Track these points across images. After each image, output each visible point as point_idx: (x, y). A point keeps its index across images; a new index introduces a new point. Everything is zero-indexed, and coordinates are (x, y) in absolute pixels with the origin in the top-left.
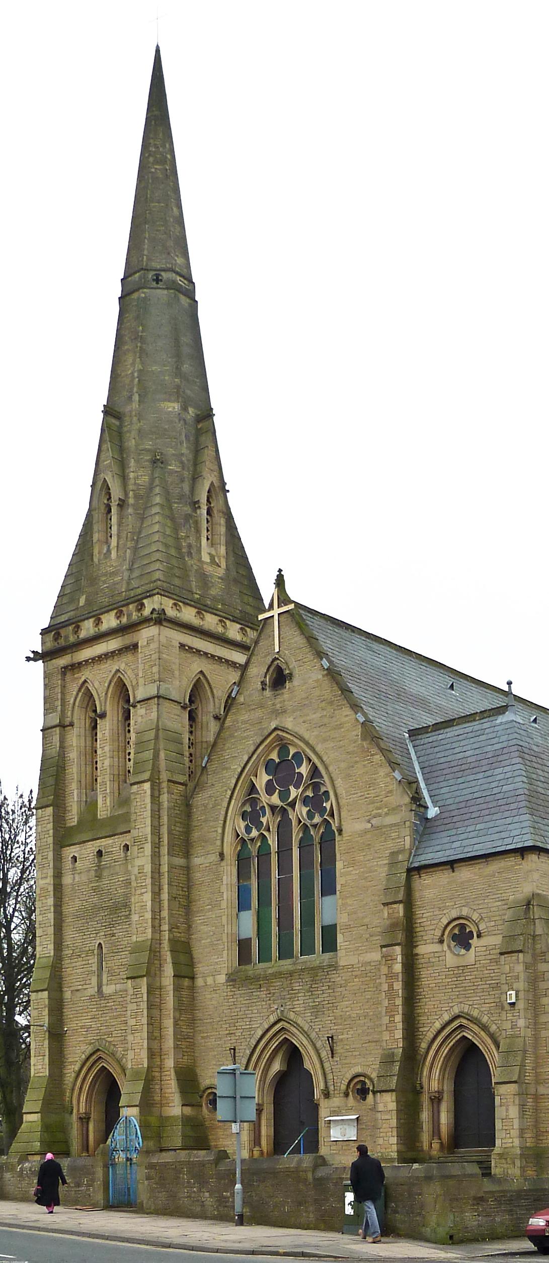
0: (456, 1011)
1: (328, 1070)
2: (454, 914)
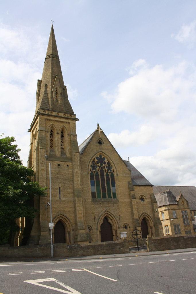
0: (143, 212)
1: (119, 222)
2: (141, 194)
